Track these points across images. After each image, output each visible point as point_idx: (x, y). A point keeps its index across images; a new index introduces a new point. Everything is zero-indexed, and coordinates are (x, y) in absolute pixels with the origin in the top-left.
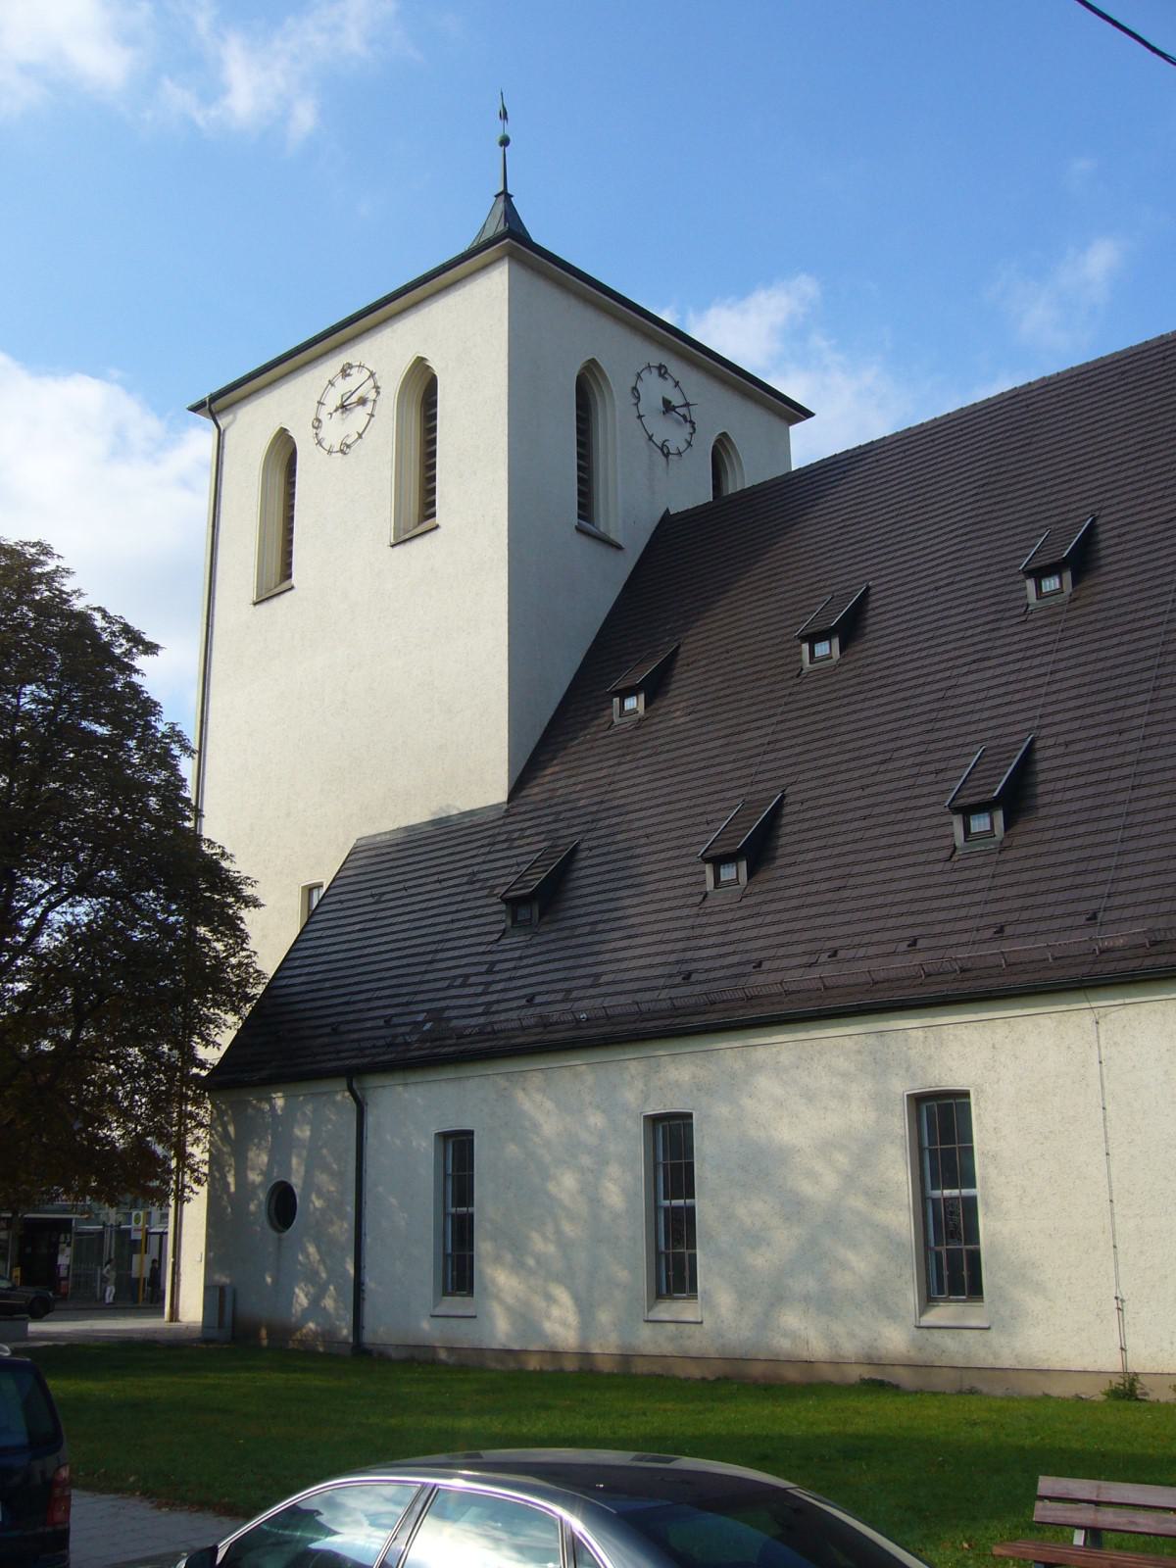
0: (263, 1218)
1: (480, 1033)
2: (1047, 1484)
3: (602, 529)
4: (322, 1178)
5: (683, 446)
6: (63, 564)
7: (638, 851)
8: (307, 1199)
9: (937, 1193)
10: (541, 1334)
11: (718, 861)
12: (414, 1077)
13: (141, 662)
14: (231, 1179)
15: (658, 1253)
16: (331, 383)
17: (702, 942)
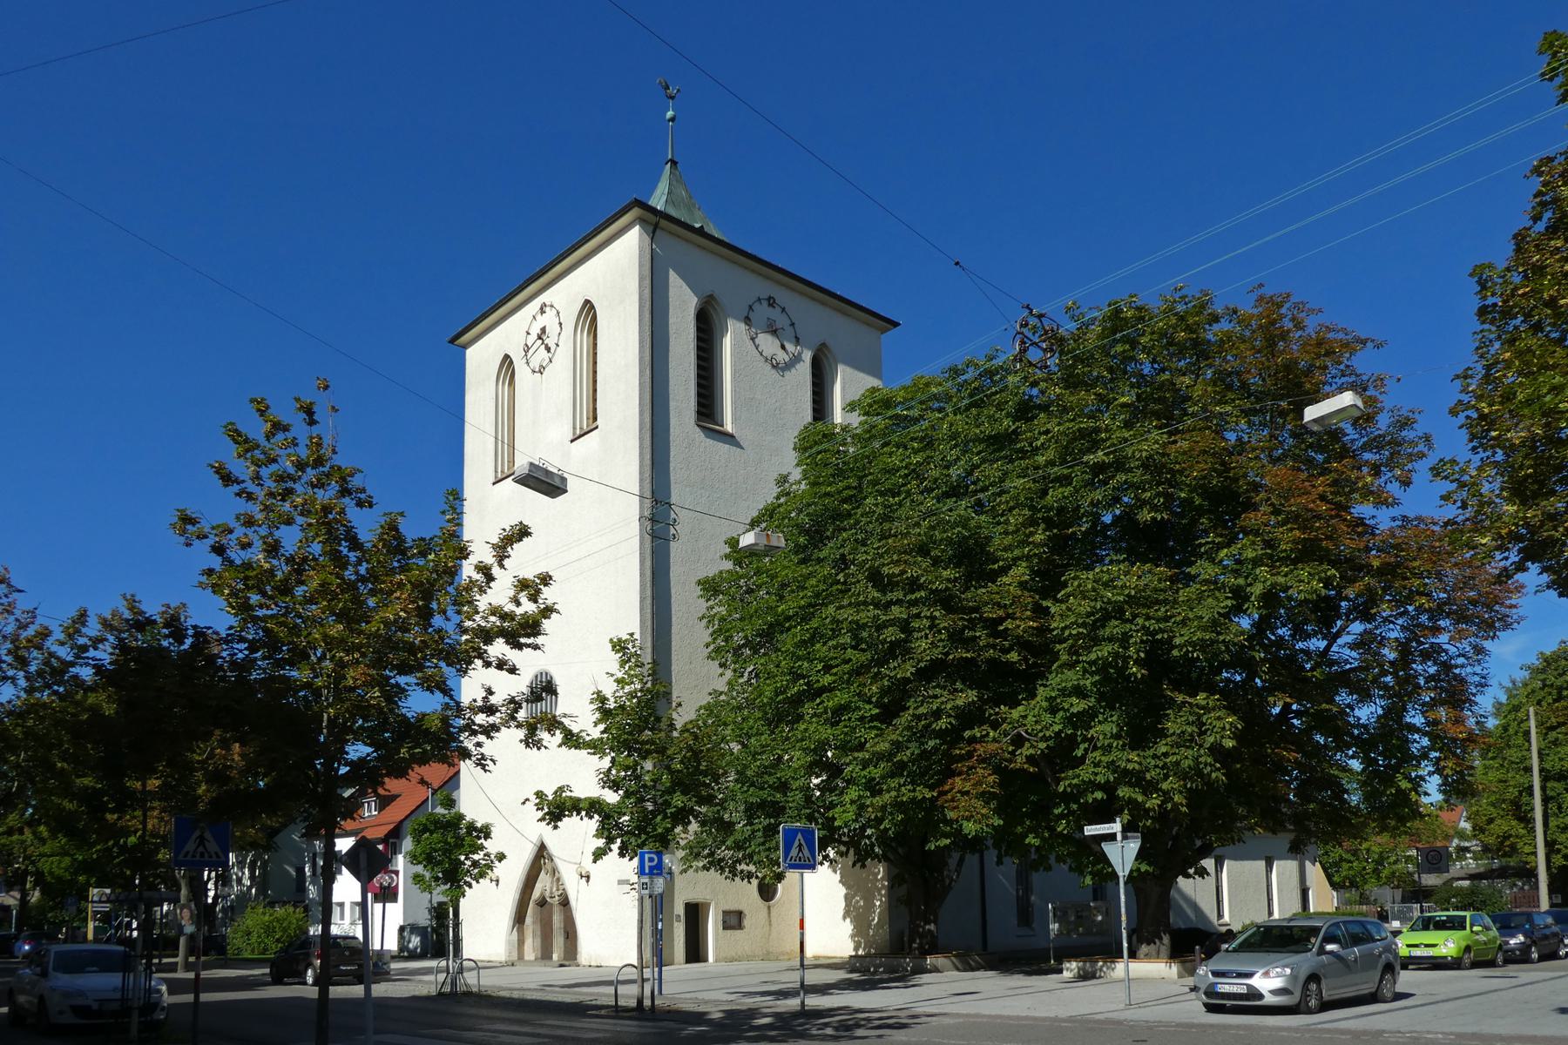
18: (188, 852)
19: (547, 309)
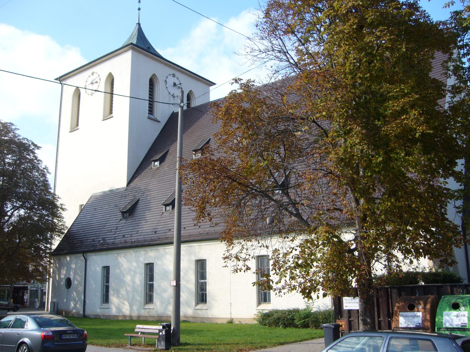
0: (64, 286)
1: (112, 244)
2: (138, 326)
3: (155, 117)
4: (77, 277)
6: (17, 127)
7: (151, 201)
8: (74, 282)
9: (200, 281)
10: (122, 312)
11: (166, 205)
12: (97, 253)
13: (36, 151)
14: (57, 277)
15: (147, 294)
16: (89, 76)
17: (160, 224)
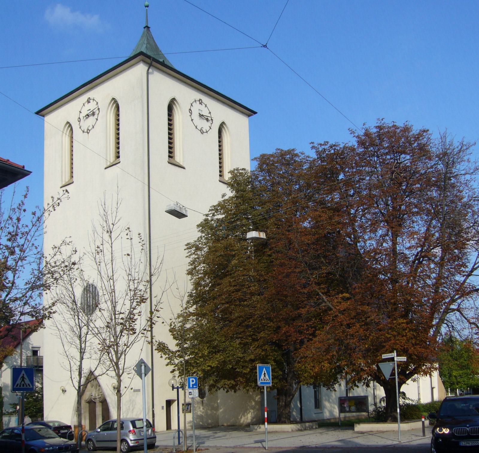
5: (208, 129)
18: (18, 384)
19: (91, 101)
